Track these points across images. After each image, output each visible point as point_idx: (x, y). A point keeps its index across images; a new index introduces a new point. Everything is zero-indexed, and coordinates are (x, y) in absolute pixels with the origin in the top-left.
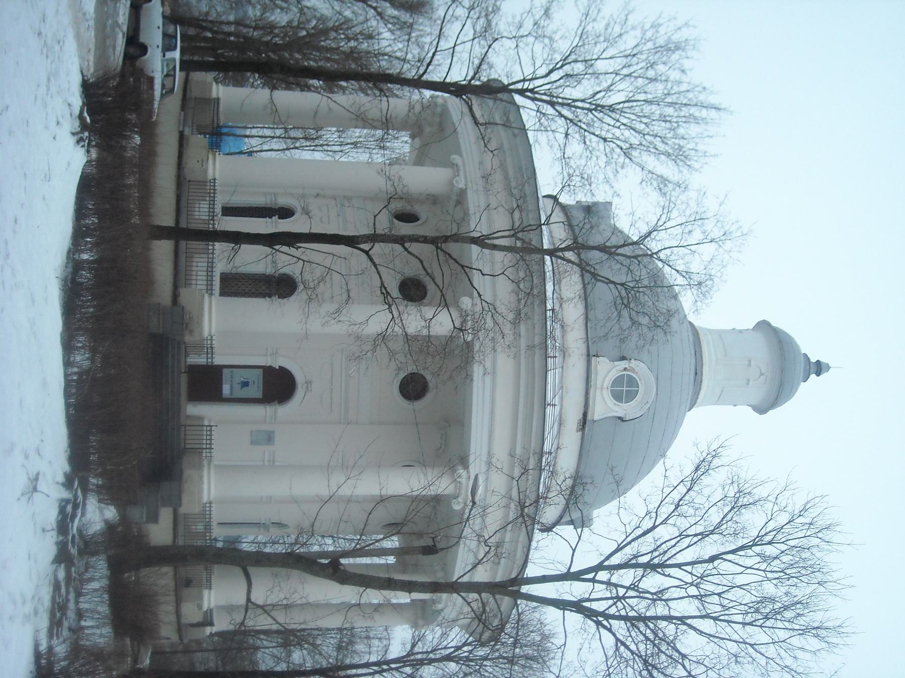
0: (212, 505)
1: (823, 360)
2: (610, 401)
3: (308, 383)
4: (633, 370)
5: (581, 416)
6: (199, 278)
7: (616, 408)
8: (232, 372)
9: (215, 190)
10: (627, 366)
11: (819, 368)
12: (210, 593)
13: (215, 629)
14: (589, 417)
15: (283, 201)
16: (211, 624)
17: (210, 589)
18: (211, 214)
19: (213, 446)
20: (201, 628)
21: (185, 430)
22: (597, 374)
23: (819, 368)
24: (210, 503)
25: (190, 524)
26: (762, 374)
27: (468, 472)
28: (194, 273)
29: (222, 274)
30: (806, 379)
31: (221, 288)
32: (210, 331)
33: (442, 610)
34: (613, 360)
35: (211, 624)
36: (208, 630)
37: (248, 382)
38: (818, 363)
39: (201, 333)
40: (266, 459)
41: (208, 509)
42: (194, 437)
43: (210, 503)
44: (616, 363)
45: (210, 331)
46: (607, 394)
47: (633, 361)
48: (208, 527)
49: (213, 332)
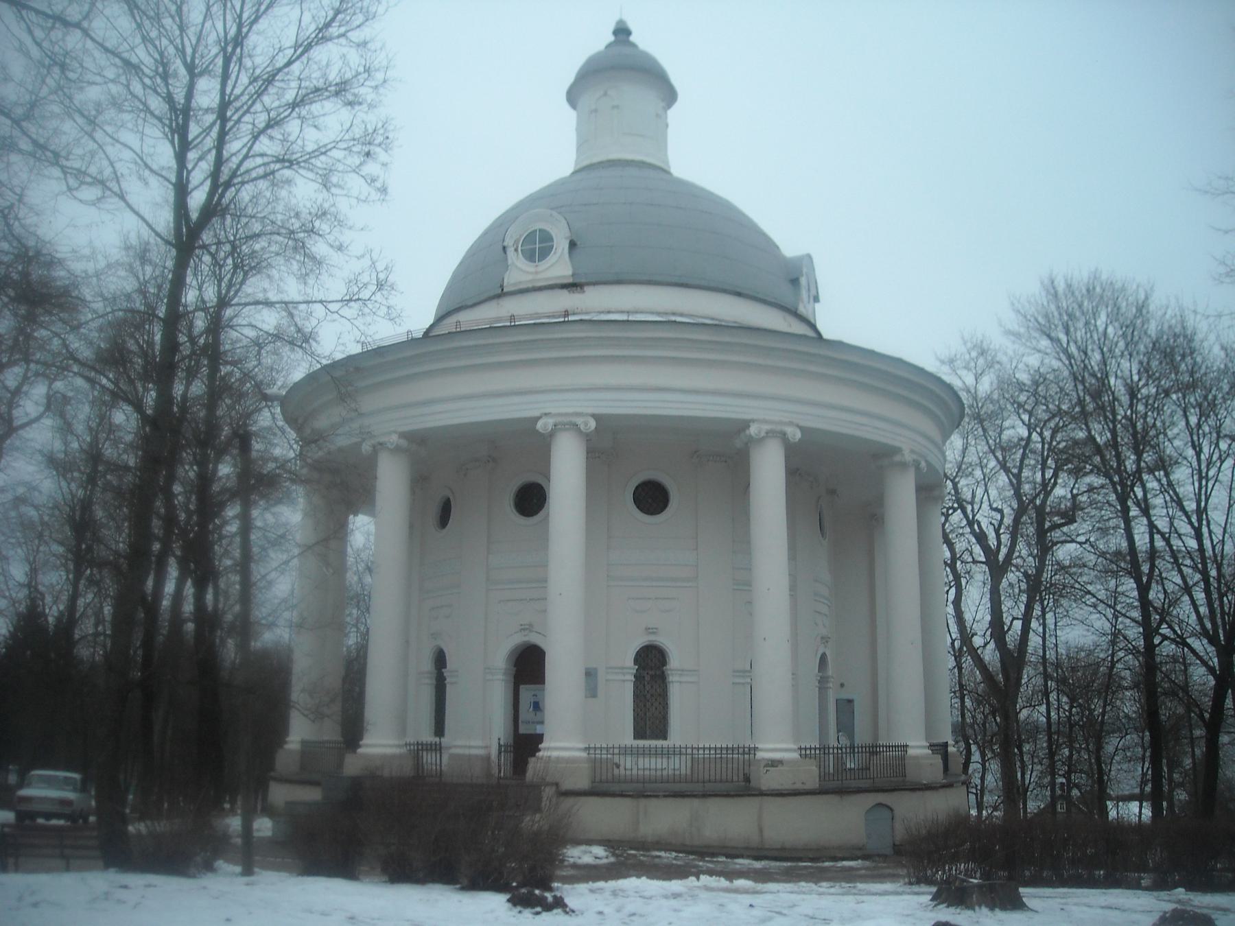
0: (803, 746)
1: (612, 27)
2: (552, 258)
3: (649, 631)
4: (516, 242)
5: (565, 292)
6: (653, 766)
7: (559, 251)
8: (522, 722)
9: (811, 749)
10: (513, 249)
11: (622, 32)
12: (762, 750)
13: (951, 742)
14: (571, 280)
15: (428, 665)
16: (946, 745)
17: (755, 749)
18: (684, 750)
19: (730, 746)
20: (950, 758)
21: (710, 781)
22: (520, 282)
23: (622, 32)
24: (406, 744)
25: (610, 775)
26: (605, 94)
27: (753, 421)
28: (641, 772)
29: (635, 738)
30: (634, 45)
31: (657, 737)
32: (579, 749)
33: (801, 428)
34: (507, 267)
35: (946, 745)
36: (951, 749)
37: (534, 702)
38: (616, 32)
39: (400, 756)
40: (621, 677)
41: (808, 752)
42: (724, 770)
43: (801, 749)
44: (510, 262)
45: (579, 749)
46: (544, 265)
47: (505, 244)
48: (429, 747)
49: (582, 746)
